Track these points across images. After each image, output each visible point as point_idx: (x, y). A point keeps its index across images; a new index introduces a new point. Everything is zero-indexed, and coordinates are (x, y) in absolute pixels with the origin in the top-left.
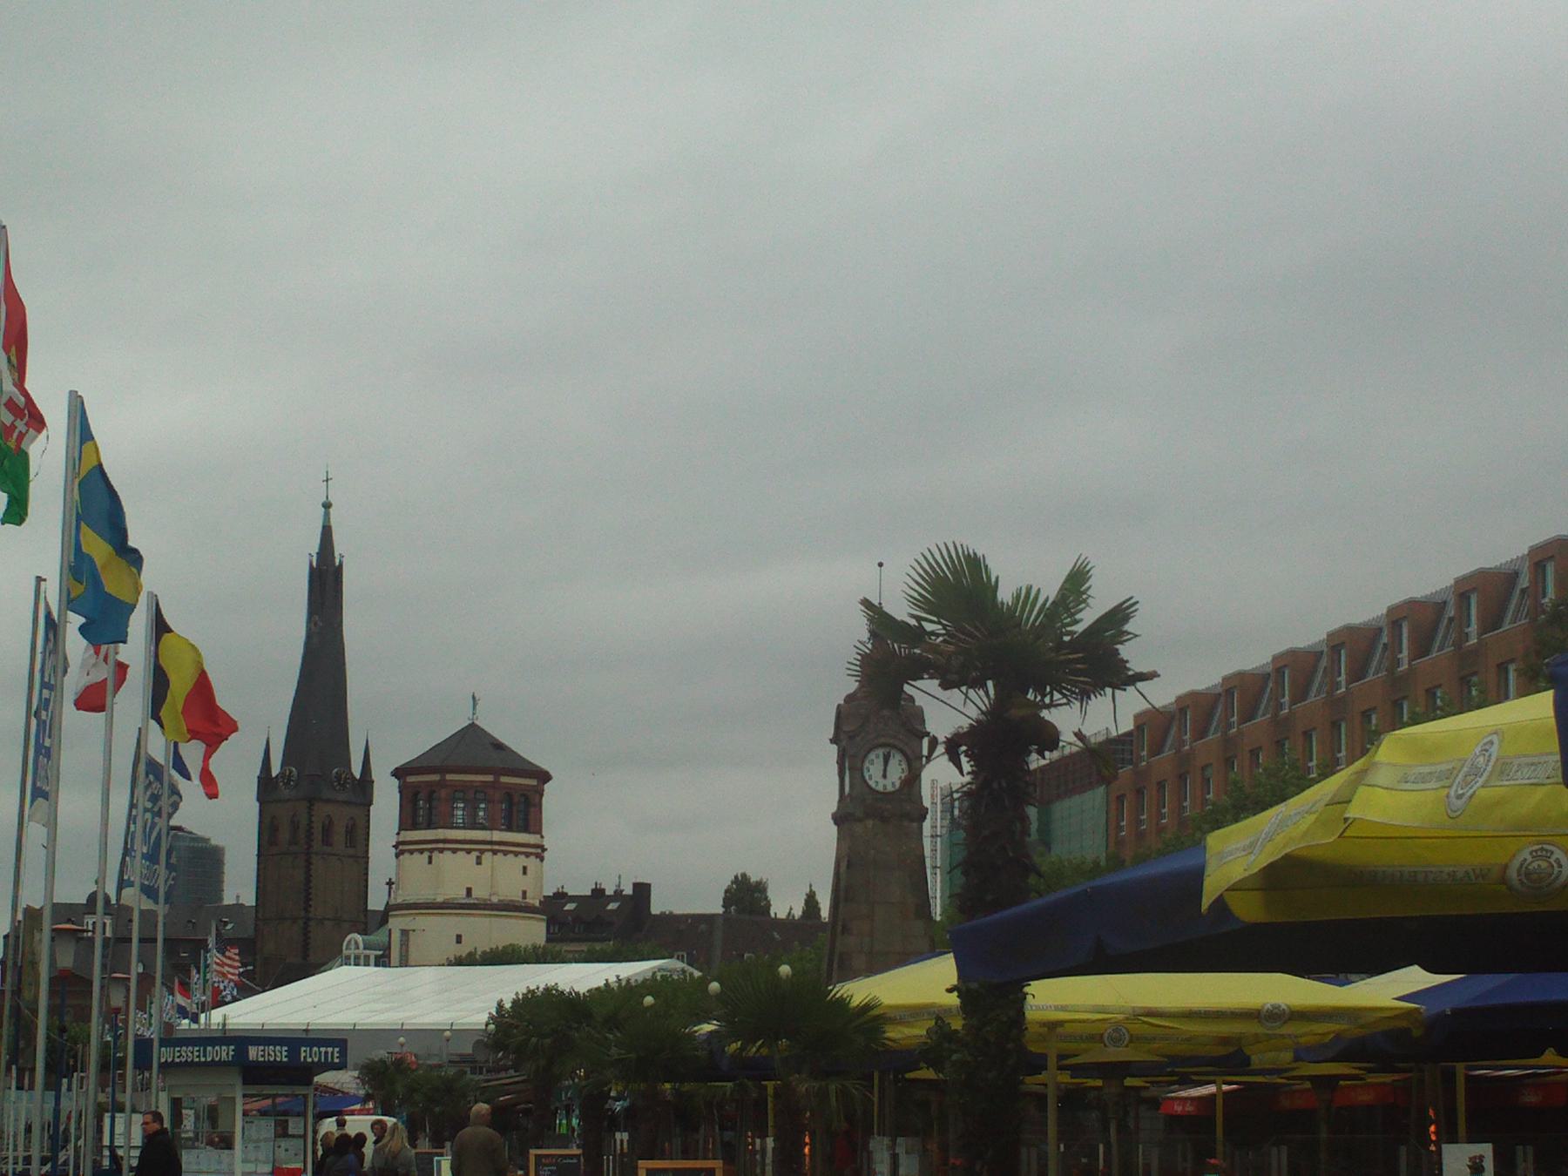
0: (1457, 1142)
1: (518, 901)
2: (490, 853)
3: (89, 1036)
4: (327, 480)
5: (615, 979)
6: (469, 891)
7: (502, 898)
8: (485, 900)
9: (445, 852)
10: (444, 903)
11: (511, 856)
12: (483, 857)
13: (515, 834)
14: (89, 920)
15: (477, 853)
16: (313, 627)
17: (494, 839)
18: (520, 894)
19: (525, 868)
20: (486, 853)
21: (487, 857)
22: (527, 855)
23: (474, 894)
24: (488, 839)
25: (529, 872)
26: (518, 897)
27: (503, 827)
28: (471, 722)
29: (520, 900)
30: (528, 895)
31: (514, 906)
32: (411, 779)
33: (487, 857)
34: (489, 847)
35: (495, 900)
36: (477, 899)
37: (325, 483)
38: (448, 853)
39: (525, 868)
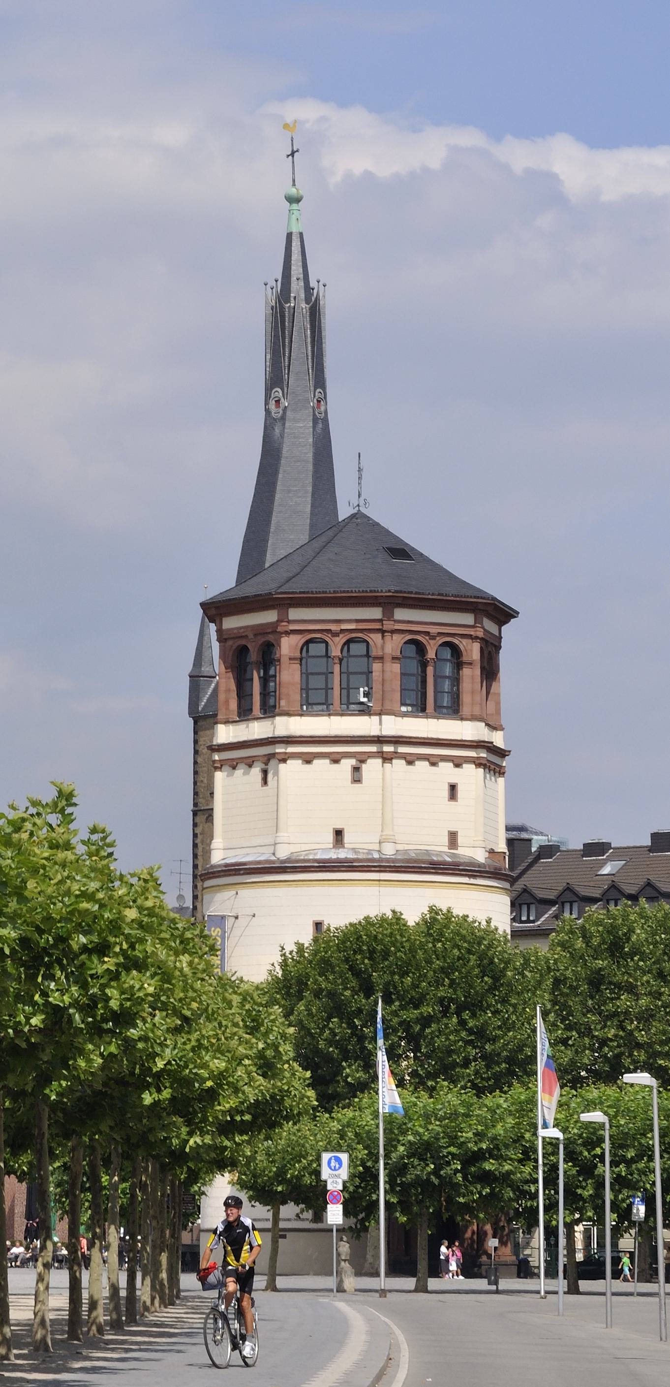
0: (199, 1246)
1: (440, 853)
2: (379, 761)
3: (604, 1181)
4: (292, 154)
5: (294, 948)
6: (453, 837)
7: (400, 847)
8: (370, 851)
9: (316, 762)
10: (288, 860)
11: (422, 766)
12: (364, 767)
13: (432, 722)
14: (455, 1020)
15: (353, 762)
16: (272, 406)
17: (385, 732)
18: (445, 840)
19: (453, 788)
20: (369, 761)
21: (372, 767)
22: (458, 763)
23: (348, 838)
24: (375, 731)
25: (461, 792)
26: (438, 847)
27: (404, 709)
28: (355, 511)
29: (446, 849)
30: (460, 840)
31: (432, 863)
32: (231, 623)
33: (372, 767)
34: (373, 748)
35: (389, 851)
36: (354, 850)
37: (290, 157)
38: (399, 763)
39: (453, 788)
